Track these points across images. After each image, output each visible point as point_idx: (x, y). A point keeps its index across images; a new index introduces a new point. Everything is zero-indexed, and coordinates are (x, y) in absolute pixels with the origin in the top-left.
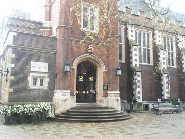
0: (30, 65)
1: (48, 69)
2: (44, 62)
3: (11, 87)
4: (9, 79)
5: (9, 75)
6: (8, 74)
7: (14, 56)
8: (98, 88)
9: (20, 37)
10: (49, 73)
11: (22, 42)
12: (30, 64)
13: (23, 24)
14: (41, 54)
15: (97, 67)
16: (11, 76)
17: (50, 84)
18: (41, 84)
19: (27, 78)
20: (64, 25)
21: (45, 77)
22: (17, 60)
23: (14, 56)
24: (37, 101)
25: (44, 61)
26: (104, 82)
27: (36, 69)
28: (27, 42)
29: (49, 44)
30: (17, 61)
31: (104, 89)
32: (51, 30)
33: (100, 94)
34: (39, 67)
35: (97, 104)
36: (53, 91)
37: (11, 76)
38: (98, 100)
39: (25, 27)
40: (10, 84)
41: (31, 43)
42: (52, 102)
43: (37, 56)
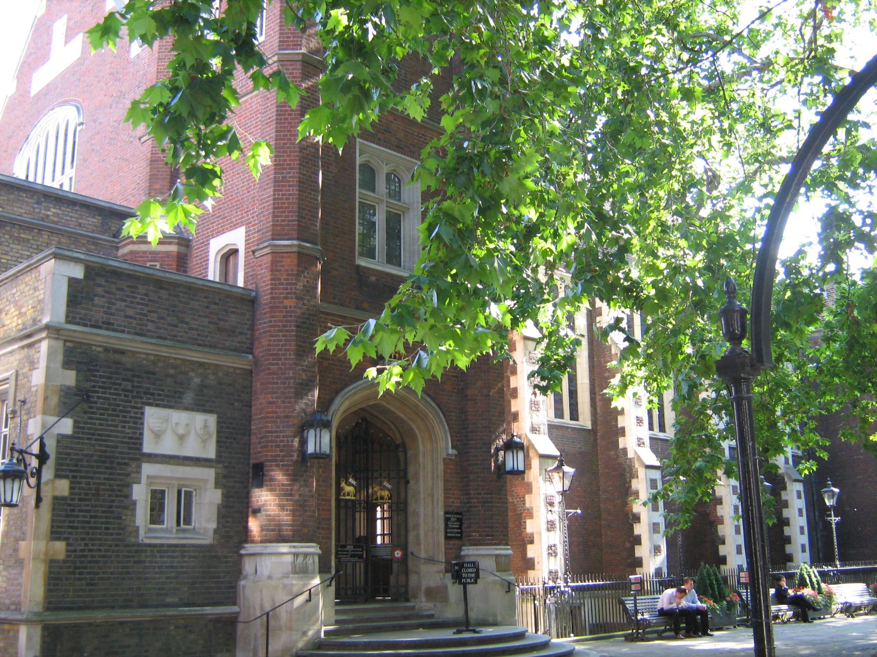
0: (142, 424)
1: (218, 442)
2: (198, 410)
3: (55, 534)
4: (47, 494)
5: (48, 473)
6: (45, 468)
7: (70, 378)
8: (422, 532)
9: (100, 285)
10: (220, 465)
11: (106, 313)
12: (138, 421)
13: (48, 216)
14: (186, 373)
15: (414, 437)
16: (58, 476)
17: (224, 517)
18: (184, 516)
19: (129, 486)
20: (298, 239)
21: (206, 481)
22: (88, 400)
23: (70, 378)
24: (169, 600)
25: (200, 407)
26: (446, 505)
27: (168, 446)
28: (130, 312)
29: (222, 324)
30: (85, 406)
31: (447, 538)
32: (183, 249)
33: (431, 560)
34: (176, 432)
35: (413, 608)
36: (237, 552)
37: (58, 476)
38: (423, 587)
39: (53, 232)
40: (53, 521)
41: (146, 315)
42: (235, 604)
43: (169, 380)
